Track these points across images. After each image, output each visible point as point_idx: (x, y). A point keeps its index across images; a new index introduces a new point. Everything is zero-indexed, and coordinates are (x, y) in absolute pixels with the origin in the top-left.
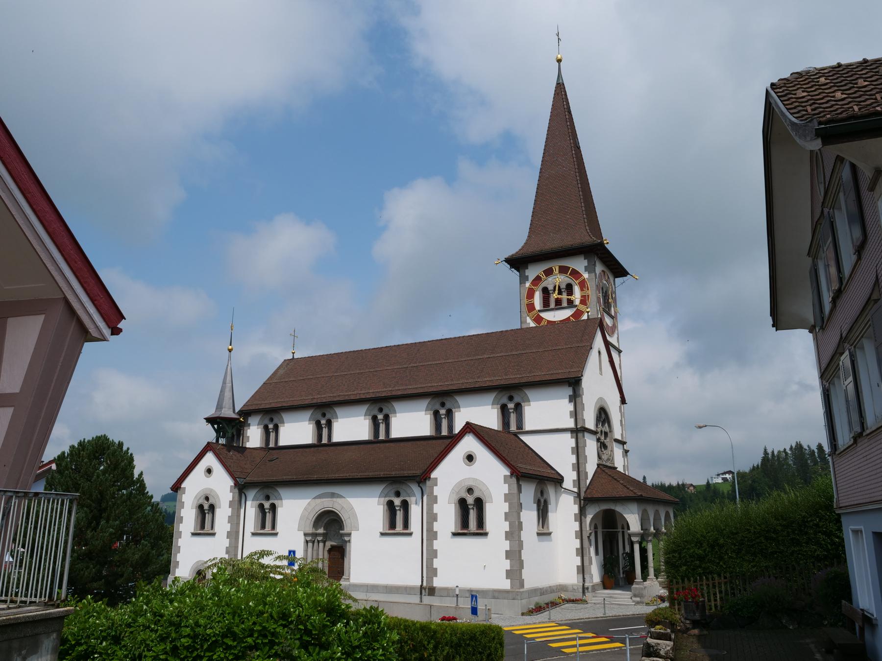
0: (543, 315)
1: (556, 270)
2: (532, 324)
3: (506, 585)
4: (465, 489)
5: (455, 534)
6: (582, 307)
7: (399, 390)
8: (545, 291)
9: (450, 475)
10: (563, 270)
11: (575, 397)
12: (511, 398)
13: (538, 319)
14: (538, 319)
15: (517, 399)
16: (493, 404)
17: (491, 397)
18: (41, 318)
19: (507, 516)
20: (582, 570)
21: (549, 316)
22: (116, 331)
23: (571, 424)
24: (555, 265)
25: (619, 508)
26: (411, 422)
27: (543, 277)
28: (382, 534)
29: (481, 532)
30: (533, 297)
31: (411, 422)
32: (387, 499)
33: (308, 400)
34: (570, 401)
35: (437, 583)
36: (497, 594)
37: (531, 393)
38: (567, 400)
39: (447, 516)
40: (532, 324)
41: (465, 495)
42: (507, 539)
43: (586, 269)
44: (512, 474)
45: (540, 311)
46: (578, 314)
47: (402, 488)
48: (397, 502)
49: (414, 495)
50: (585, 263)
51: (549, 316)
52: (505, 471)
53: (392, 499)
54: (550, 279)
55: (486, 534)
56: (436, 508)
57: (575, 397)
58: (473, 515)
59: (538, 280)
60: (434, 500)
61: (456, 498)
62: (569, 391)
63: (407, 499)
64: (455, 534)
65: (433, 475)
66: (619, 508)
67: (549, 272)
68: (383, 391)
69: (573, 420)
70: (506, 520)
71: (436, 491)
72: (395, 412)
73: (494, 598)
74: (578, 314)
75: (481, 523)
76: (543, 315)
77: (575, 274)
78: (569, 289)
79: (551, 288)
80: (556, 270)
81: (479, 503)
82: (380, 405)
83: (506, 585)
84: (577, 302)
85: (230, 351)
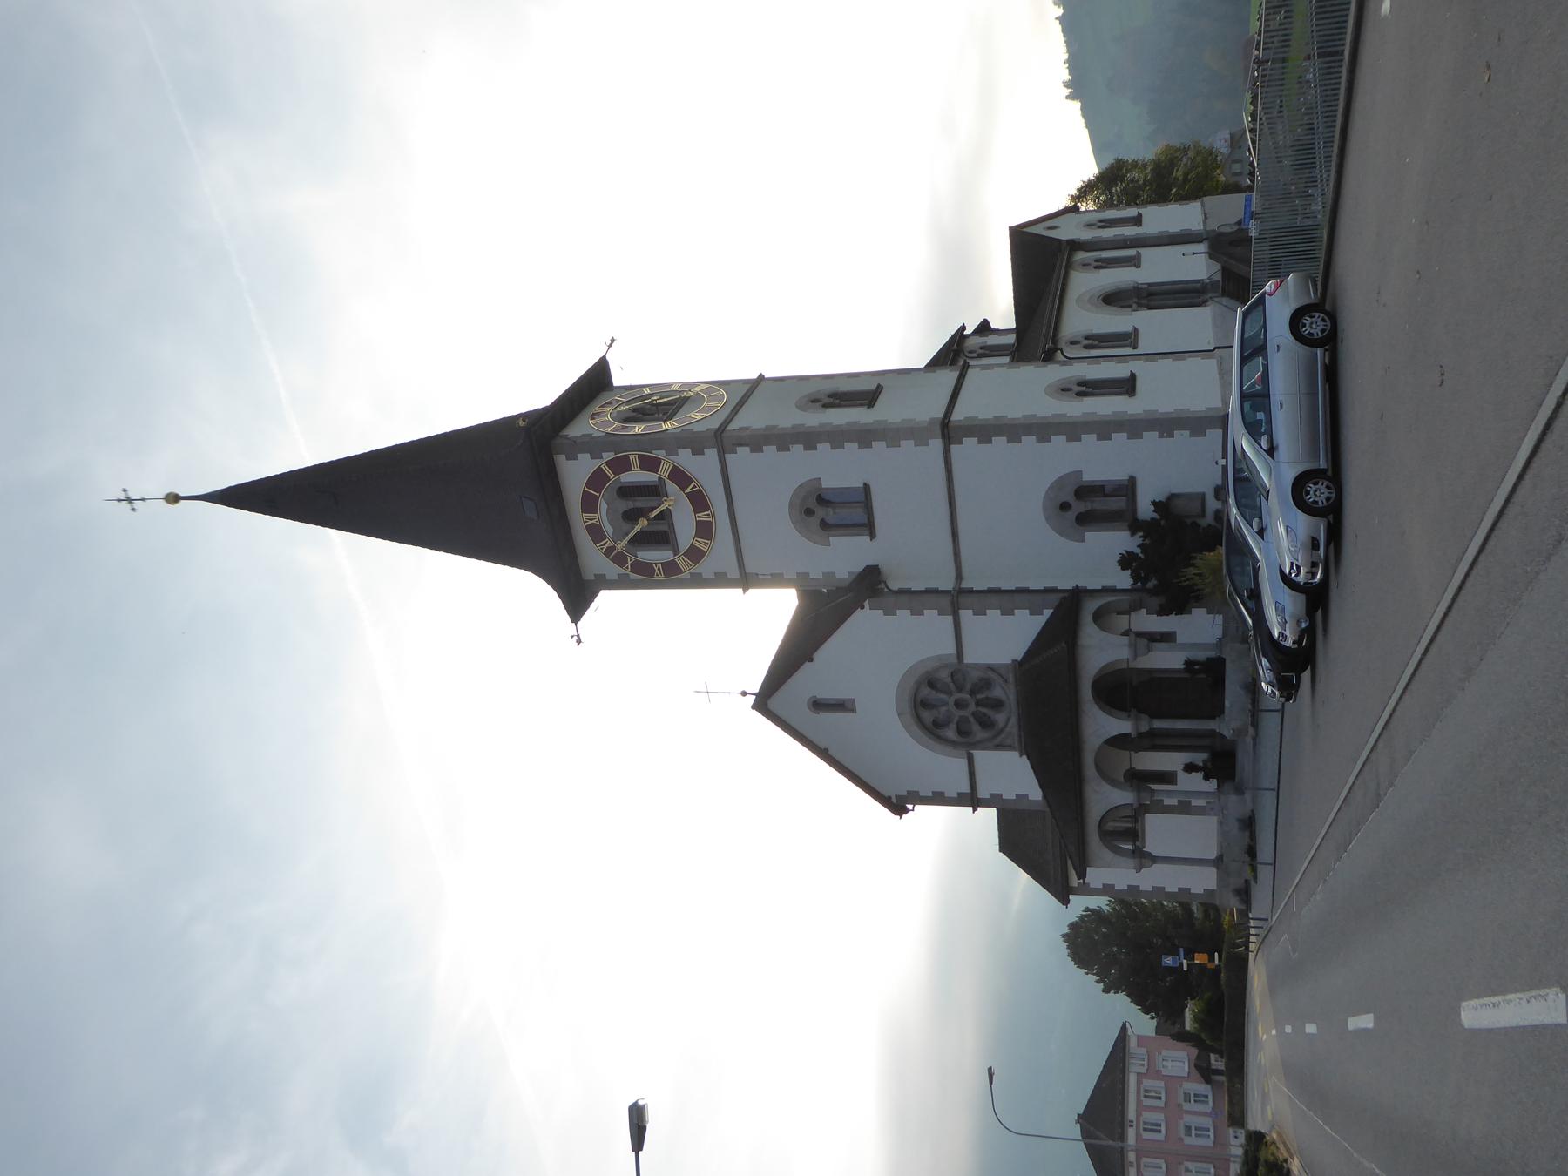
10: (589, 504)
18: (1035, 793)
24: (579, 521)
27: (608, 542)
45: (676, 552)
59: (620, 560)
77: (597, 480)
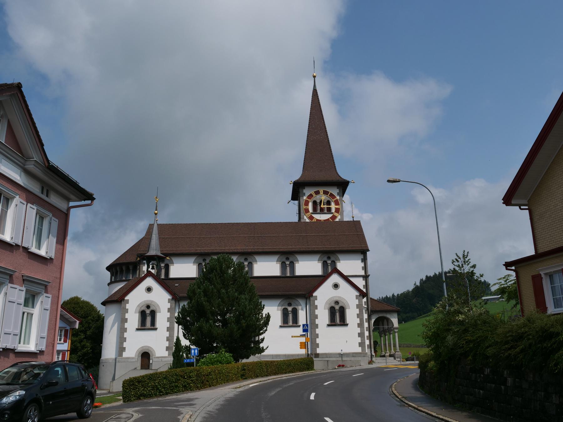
0: (314, 215)
1: (322, 192)
2: (308, 220)
3: (359, 350)
4: (333, 302)
5: (138, 329)
6: (336, 214)
7: (345, 247)
8: (315, 203)
9: (324, 295)
10: (326, 193)
11: (364, 260)
12: (204, 260)
13: (311, 218)
14: (311, 218)
15: (332, 259)
16: (194, 263)
17: (276, 257)
19: (316, 317)
20: (362, 344)
21: (317, 217)
22: (343, 185)
23: (363, 273)
25: (388, 316)
26: (308, 267)
27: (314, 195)
28: (281, 327)
29: (153, 327)
30: (308, 205)
31: (308, 267)
32: (283, 307)
33: (193, 250)
34: (362, 262)
35: (319, 351)
36: (354, 355)
37: (257, 258)
38: (360, 261)
39: (133, 319)
40: (308, 220)
41: (333, 305)
42: (358, 327)
43: (338, 194)
44: (173, 299)
45: (312, 213)
46: (334, 217)
47: (293, 302)
48: (290, 309)
49: (301, 305)
50: (338, 191)
51: (317, 217)
52: (169, 297)
53: (286, 307)
54: (318, 196)
55: (156, 329)
56: (317, 312)
57: (364, 260)
58: (290, 316)
59: (310, 196)
60: (127, 311)
61: (328, 306)
62: (362, 256)
63: (296, 307)
64: (138, 329)
65: (314, 294)
66: (388, 316)
67: (317, 193)
68: (249, 249)
69: (364, 271)
70: (358, 317)
71: (317, 303)
72: (256, 261)
73: (353, 357)
74: (334, 217)
75: (153, 323)
76: (314, 215)
77: (332, 196)
78: (329, 203)
79: (318, 201)
80: (322, 192)
81: (153, 314)
82: (287, 256)
83: (359, 350)
84: (333, 210)
85: (156, 214)
